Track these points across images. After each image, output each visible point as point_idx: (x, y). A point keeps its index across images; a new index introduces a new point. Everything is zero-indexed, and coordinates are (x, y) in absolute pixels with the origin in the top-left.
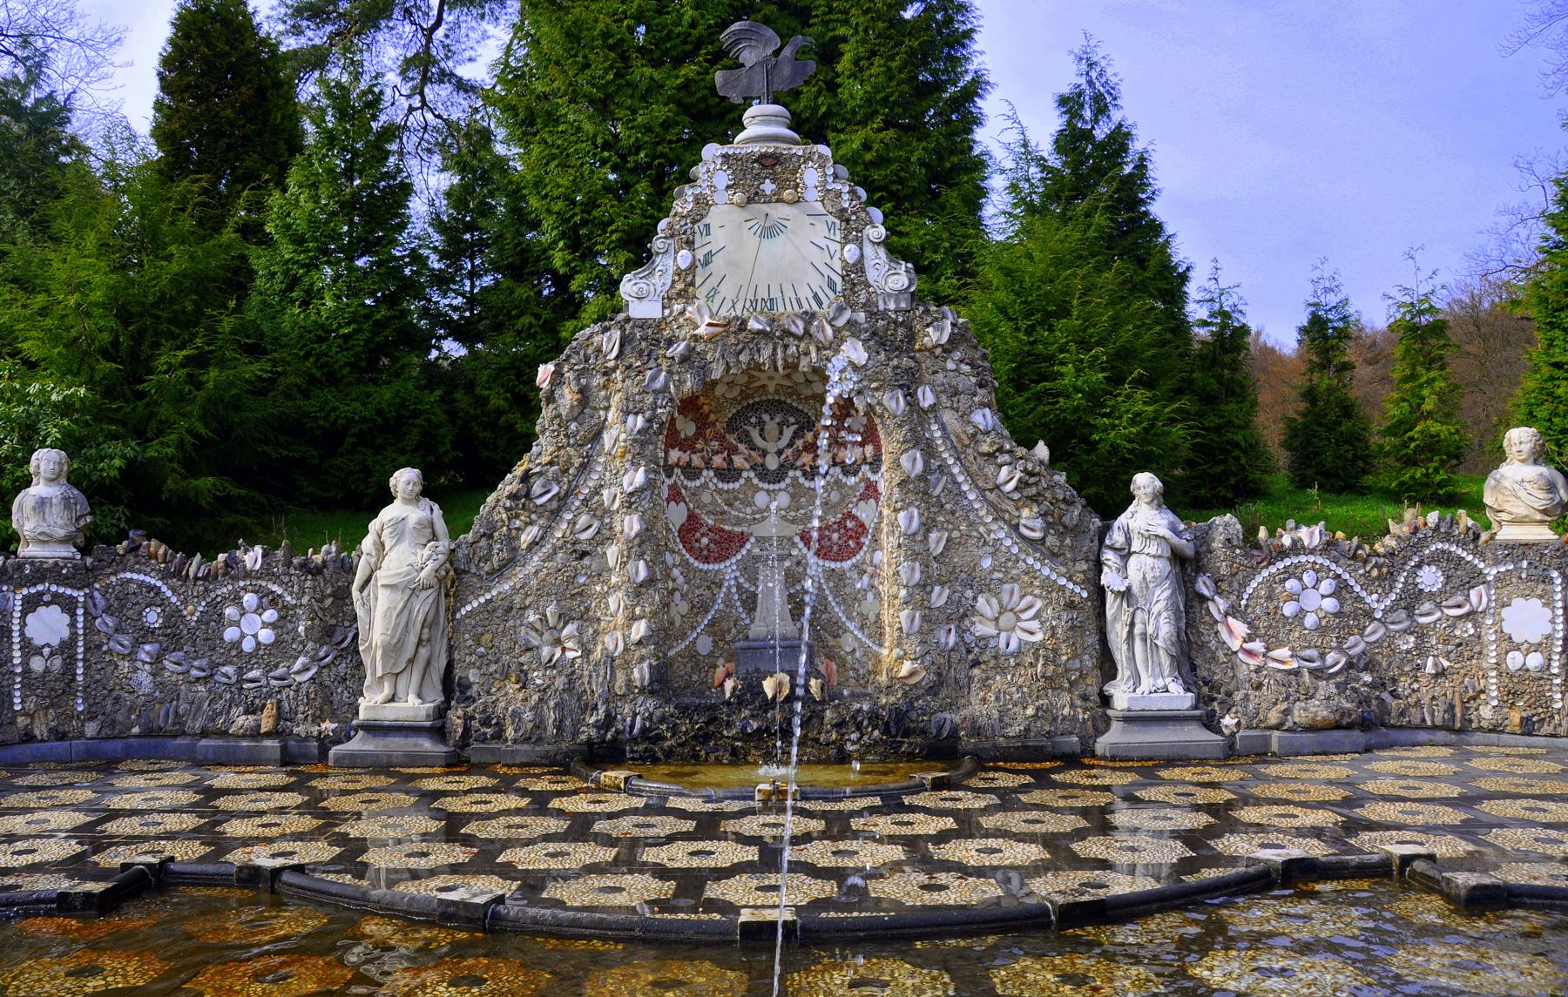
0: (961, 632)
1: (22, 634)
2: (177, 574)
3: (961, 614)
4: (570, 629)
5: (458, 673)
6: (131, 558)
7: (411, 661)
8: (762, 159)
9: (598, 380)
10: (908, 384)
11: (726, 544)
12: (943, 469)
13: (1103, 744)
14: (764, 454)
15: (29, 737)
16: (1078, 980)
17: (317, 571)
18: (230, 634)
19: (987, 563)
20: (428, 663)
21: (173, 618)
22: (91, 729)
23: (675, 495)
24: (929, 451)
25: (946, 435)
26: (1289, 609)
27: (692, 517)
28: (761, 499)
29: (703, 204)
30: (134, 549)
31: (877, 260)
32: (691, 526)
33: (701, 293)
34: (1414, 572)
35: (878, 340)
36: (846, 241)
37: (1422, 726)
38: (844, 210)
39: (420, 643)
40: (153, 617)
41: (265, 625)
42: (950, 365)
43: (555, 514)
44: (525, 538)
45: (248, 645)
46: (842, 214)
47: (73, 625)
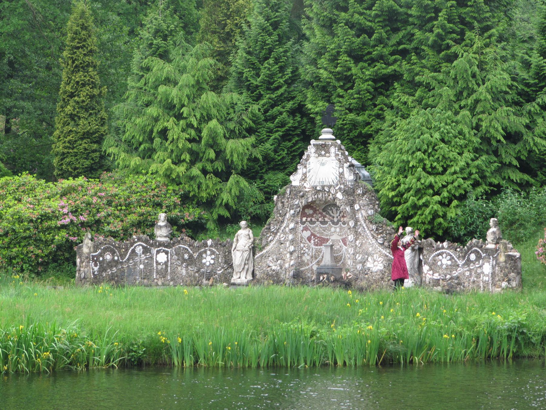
0: (363, 266)
1: (135, 247)
7: (243, 269)
14: (333, 217)
18: (212, 262)
20: (248, 270)
21: (191, 256)
28: (333, 229)
29: (308, 156)
30: (182, 239)
33: (308, 179)
34: (469, 255)
38: (339, 159)
39: (245, 264)
41: (212, 259)
42: (364, 199)
43: (276, 234)
45: (208, 264)
46: (339, 160)
47: (167, 258)
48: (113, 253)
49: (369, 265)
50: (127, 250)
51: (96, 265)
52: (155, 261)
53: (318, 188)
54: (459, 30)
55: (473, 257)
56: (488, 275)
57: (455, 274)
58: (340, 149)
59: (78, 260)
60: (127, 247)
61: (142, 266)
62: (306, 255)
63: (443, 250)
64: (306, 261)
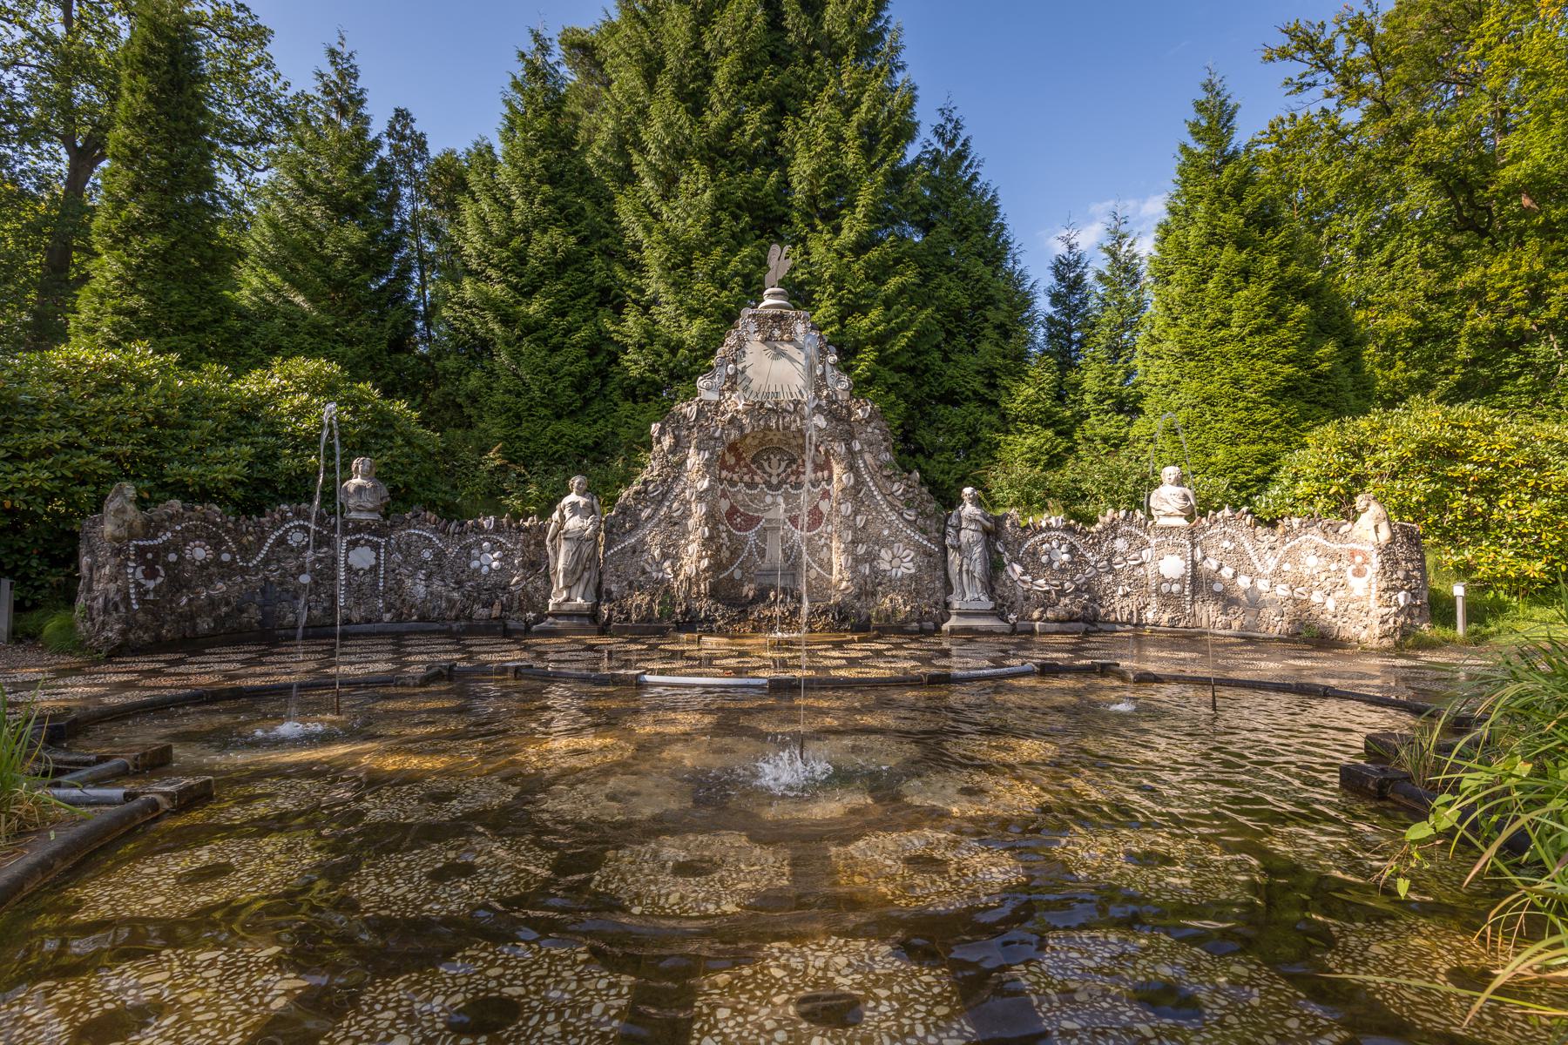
1: (286, 532)
2: (443, 531)
3: (871, 558)
4: (667, 564)
5: (605, 586)
6: (414, 522)
8: (774, 317)
9: (685, 433)
10: (849, 437)
11: (751, 522)
12: (864, 483)
13: (946, 627)
16: (241, 7)
17: (527, 530)
18: (475, 564)
19: (886, 532)
21: (439, 555)
23: (724, 495)
24: (857, 474)
25: (866, 466)
27: (732, 506)
28: (769, 499)
29: (742, 341)
31: (832, 375)
32: (732, 512)
35: (832, 416)
37: (1116, 622)
40: (427, 554)
43: (660, 503)
44: (644, 515)
47: (377, 558)
48: (217, 544)
50: (261, 540)
51: (151, 574)
59: (85, 560)
60: (263, 532)
61: (533, 490)
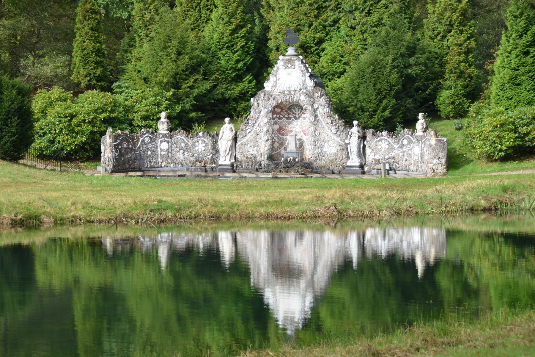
7: (228, 154)
15: (161, 167)
18: (197, 148)
21: (186, 145)
22: (172, 165)
23: (276, 123)
26: (380, 147)
33: (278, 86)
34: (402, 141)
36: (302, 76)
40: (183, 145)
42: (321, 100)
45: (200, 150)
48: (128, 142)
49: (325, 149)
50: (138, 139)
51: (117, 152)
52: (159, 148)
53: (286, 93)
54: (255, 81)
55: (405, 142)
56: (418, 155)
57: (392, 154)
58: (302, 62)
62: (276, 143)
63: (383, 138)
64: (276, 147)
